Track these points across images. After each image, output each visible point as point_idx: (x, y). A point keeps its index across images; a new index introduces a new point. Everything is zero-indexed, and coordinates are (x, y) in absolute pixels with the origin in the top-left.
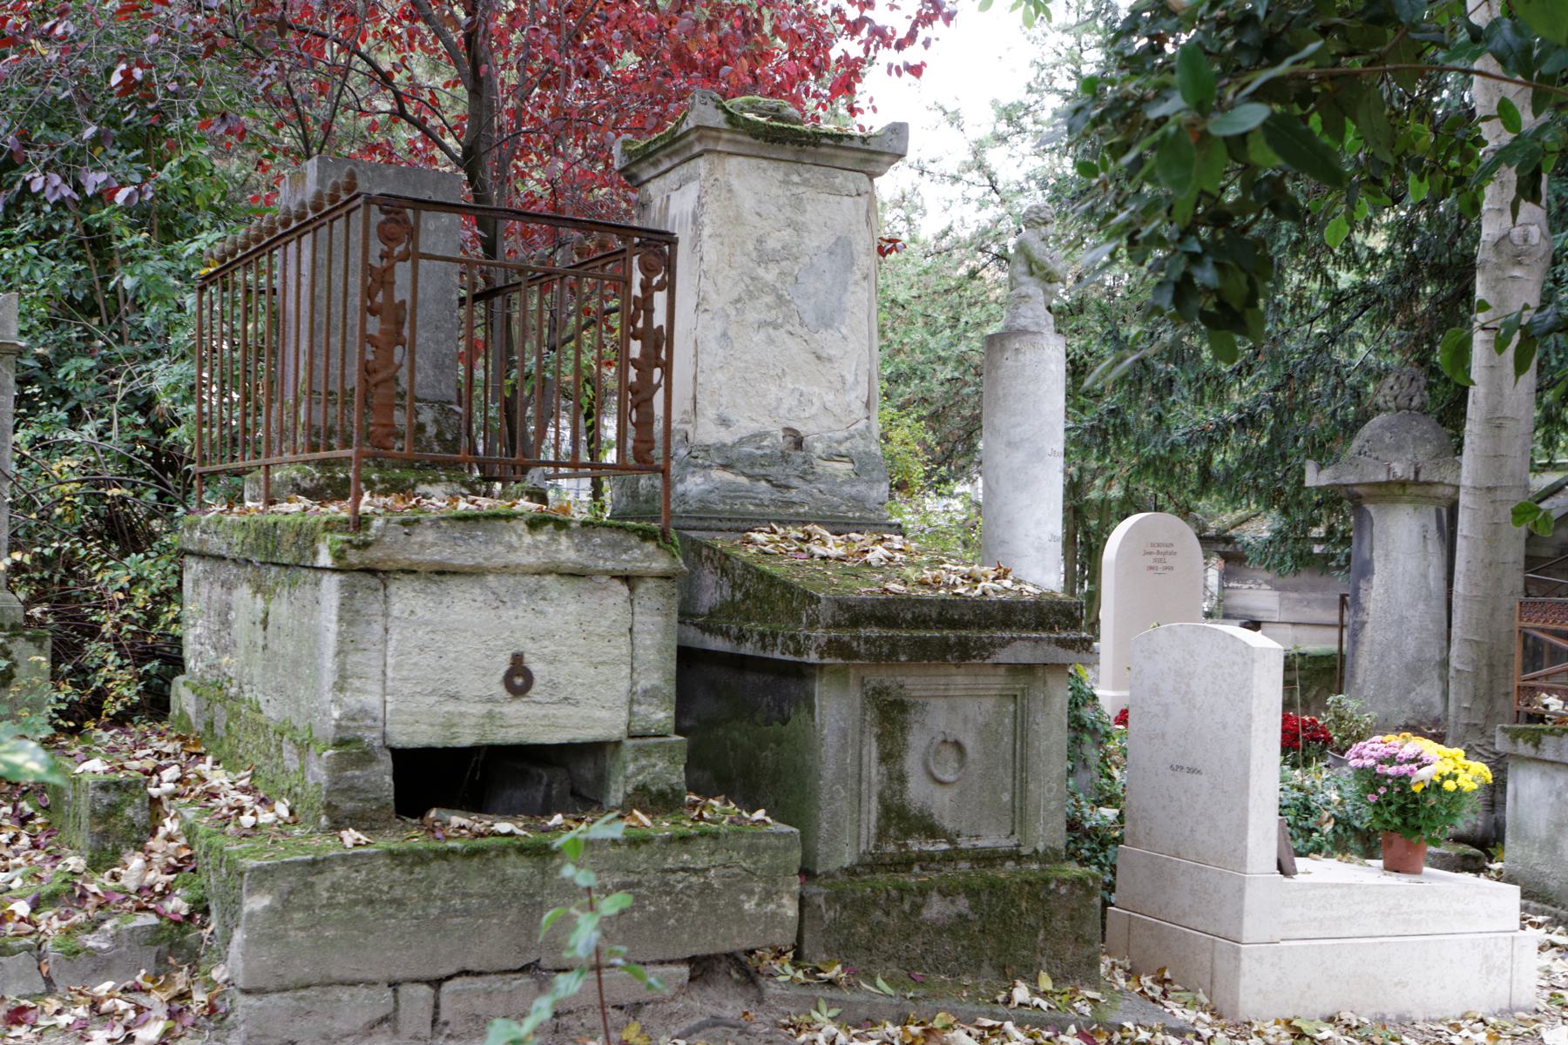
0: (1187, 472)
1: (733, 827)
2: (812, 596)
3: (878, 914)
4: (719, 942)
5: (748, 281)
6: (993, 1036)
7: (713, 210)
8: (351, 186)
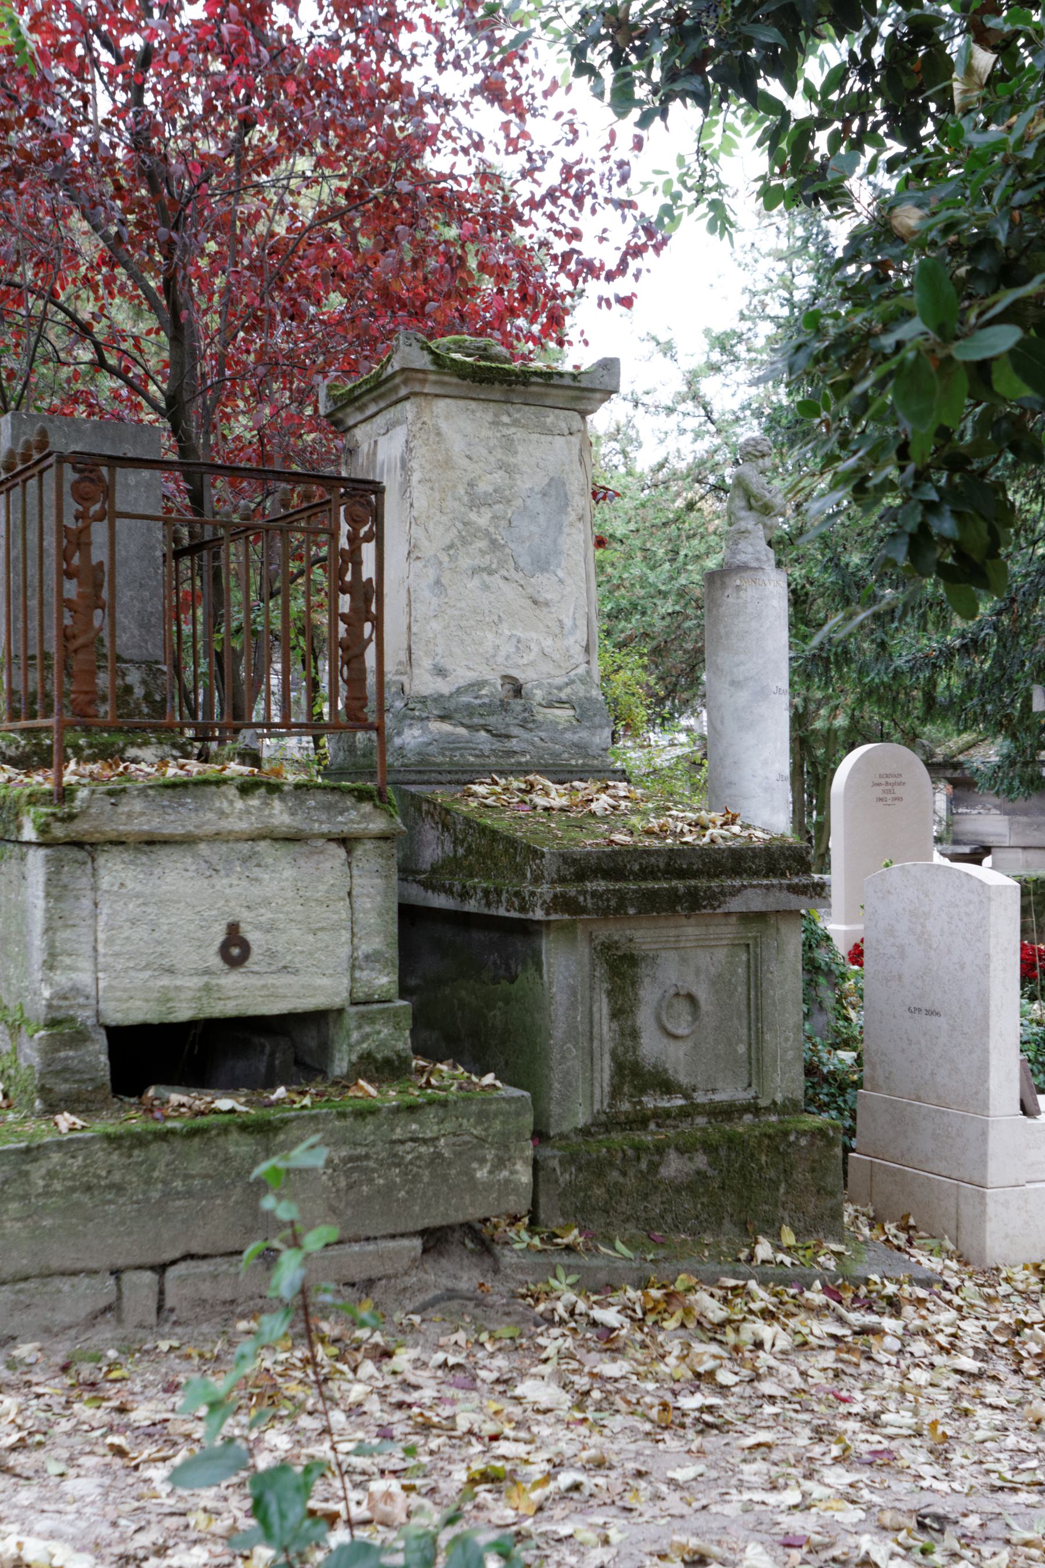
0: (910, 699)
1: (462, 1094)
2: (535, 851)
3: (614, 1175)
4: (452, 1212)
5: (460, 526)
6: (736, 1296)
7: (421, 451)
8: (43, 444)
